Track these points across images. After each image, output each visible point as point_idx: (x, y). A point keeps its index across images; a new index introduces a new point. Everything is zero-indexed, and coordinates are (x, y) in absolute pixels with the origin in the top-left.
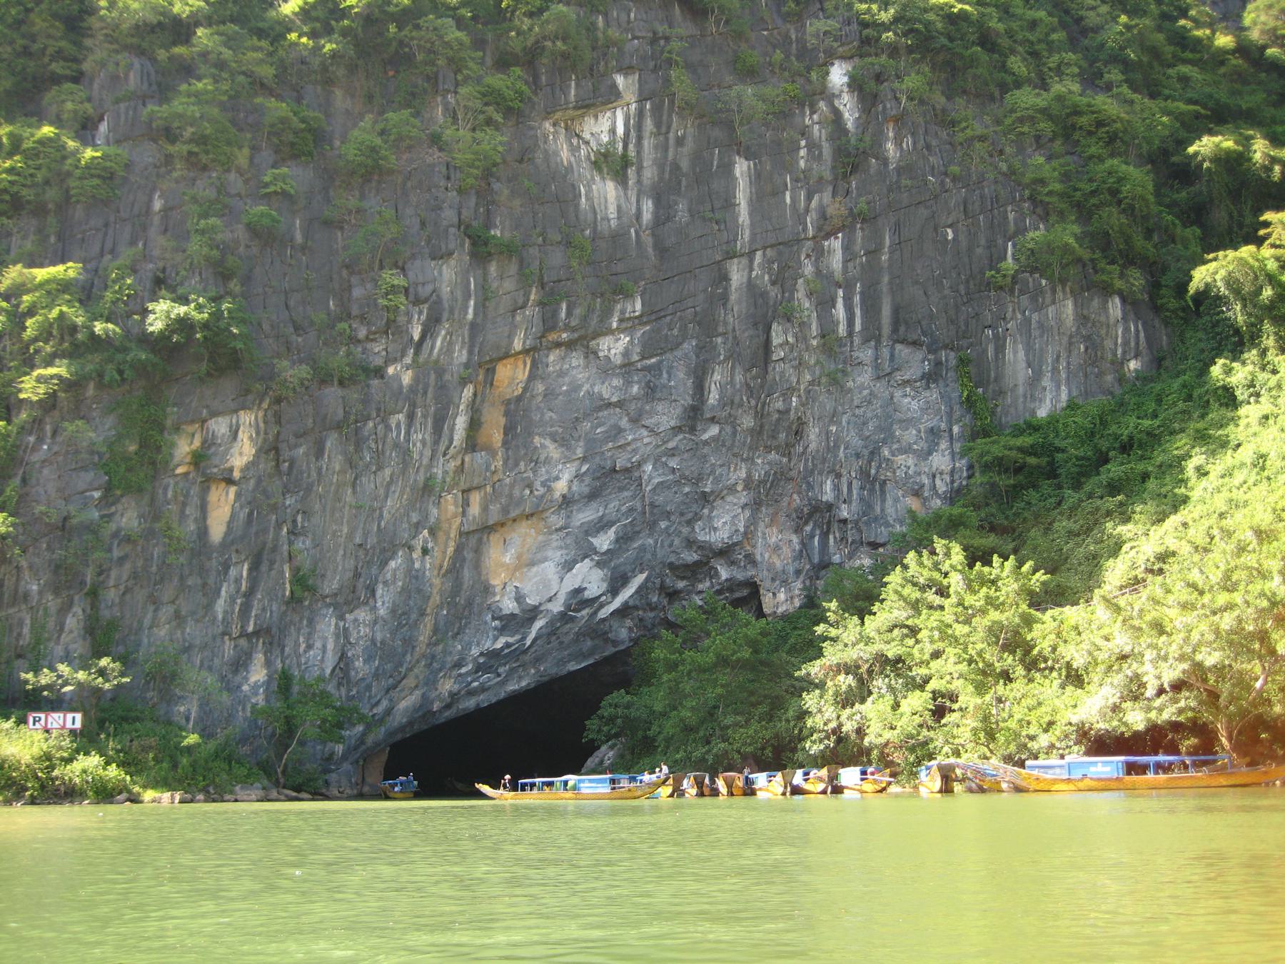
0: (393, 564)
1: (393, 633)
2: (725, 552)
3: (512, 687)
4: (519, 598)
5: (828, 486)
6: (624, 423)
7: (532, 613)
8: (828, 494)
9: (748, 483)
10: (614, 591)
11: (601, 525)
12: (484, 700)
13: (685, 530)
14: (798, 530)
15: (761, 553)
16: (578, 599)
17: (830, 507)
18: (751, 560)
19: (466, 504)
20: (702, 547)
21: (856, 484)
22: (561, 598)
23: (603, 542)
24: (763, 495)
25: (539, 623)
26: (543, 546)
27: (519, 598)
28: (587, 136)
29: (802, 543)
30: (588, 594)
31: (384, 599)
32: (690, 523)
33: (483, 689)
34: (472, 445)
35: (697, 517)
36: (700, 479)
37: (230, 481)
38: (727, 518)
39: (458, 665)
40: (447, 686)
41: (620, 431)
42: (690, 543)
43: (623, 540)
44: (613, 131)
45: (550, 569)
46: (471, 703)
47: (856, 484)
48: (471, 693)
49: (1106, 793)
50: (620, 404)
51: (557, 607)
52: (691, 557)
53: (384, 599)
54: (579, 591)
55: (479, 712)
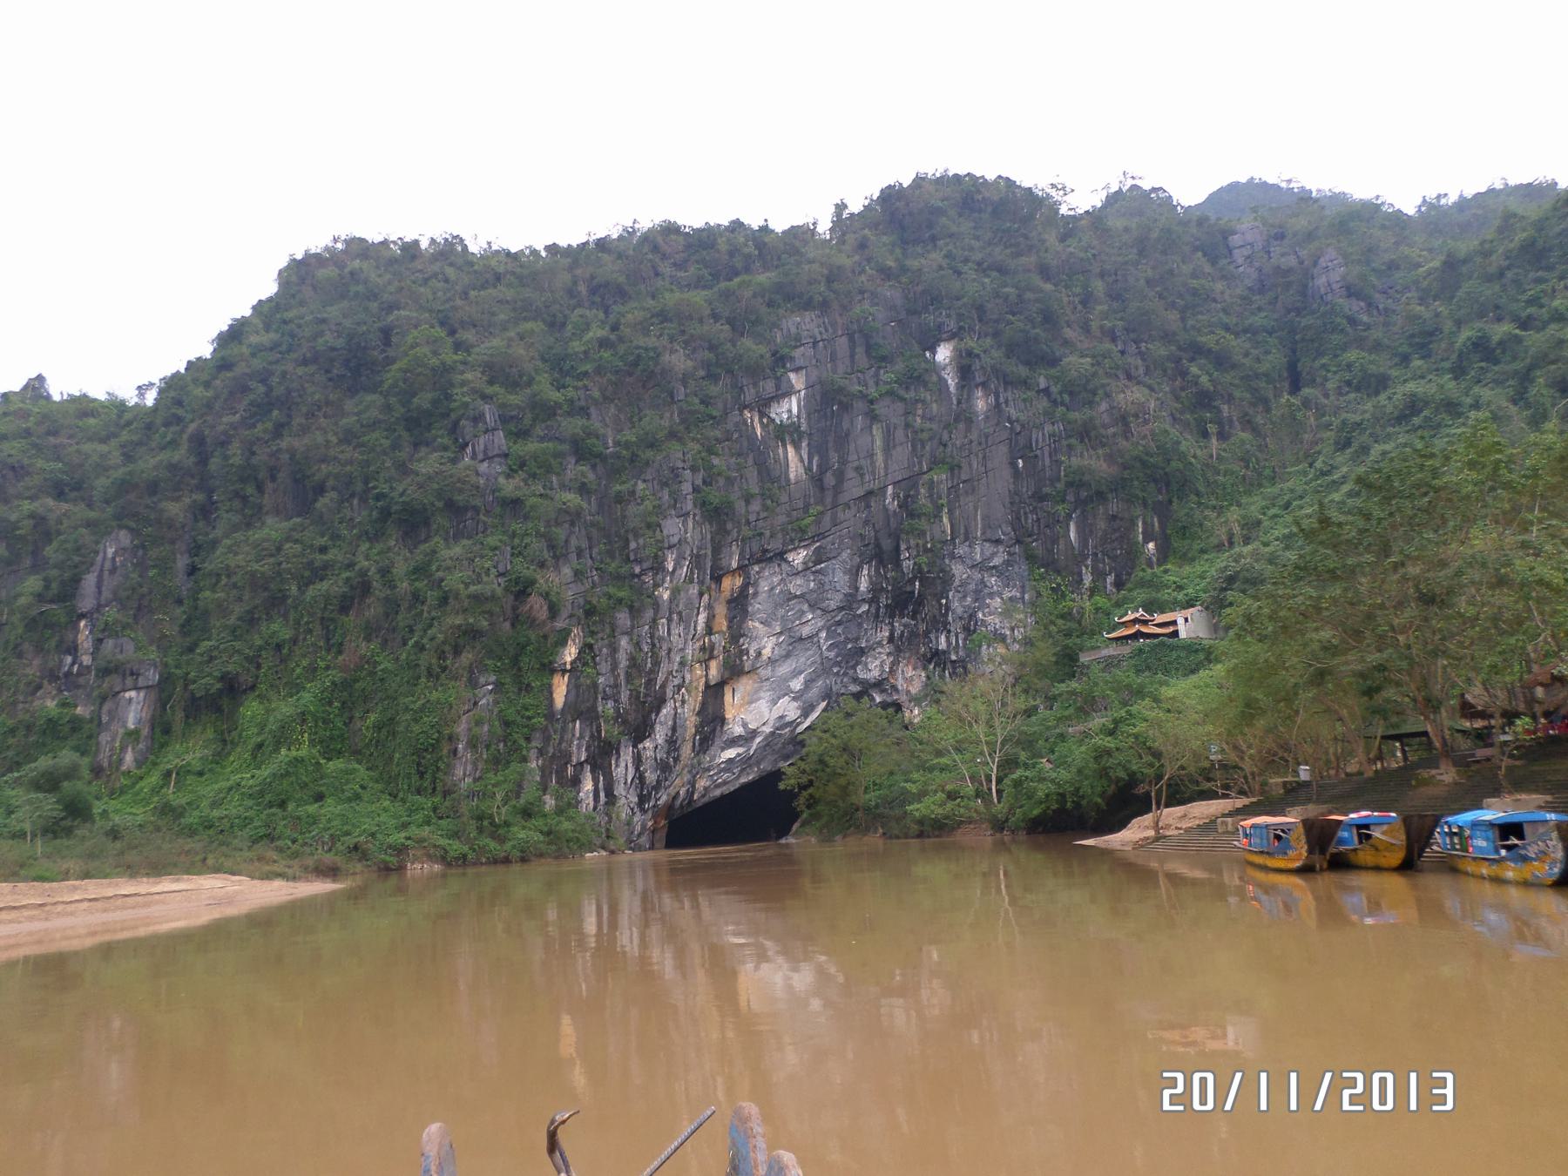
0: (664, 711)
1: (668, 753)
2: (879, 685)
3: (743, 780)
4: (745, 725)
5: (943, 639)
6: (805, 607)
7: (754, 733)
8: (943, 645)
9: (891, 639)
10: (805, 714)
11: (796, 673)
12: (726, 790)
13: (851, 672)
14: (925, 668)
15: (900, 683)
16: (782, 722)
17: (944, 652)
18: (894, 688)
19: (707, 668)
20: (863, 683)
21: (961, 636)
22: (771, 723)
23: (797, 684)
24: (899, 646)
25: (758, 740)
26: (757, 691)
27: (745, 725)
28: (773, 415)
29: (928, 677)
30: (788, 719)
31: (660, 734)
32: (854, 667)
33: (725, 783)
34: (709, 630)
35: (857, 663)
36: (857, 639)
37: (564, 671)
38: (877, 662)
39: (709, 770)
40: (702, 784)
41: (803, 613)
42: (855, 680)
43: (808, 684)
44: (790, 411)
45: (763, 705)
46: (718, 793)
47: (961, 636)
48: (718, 786)
49: (569, 1159)
50: (802, 596)
51: (767, 729)
52: (855, 688)
53: (660, 734)
54: (782, 717)
55: (723, 797)
